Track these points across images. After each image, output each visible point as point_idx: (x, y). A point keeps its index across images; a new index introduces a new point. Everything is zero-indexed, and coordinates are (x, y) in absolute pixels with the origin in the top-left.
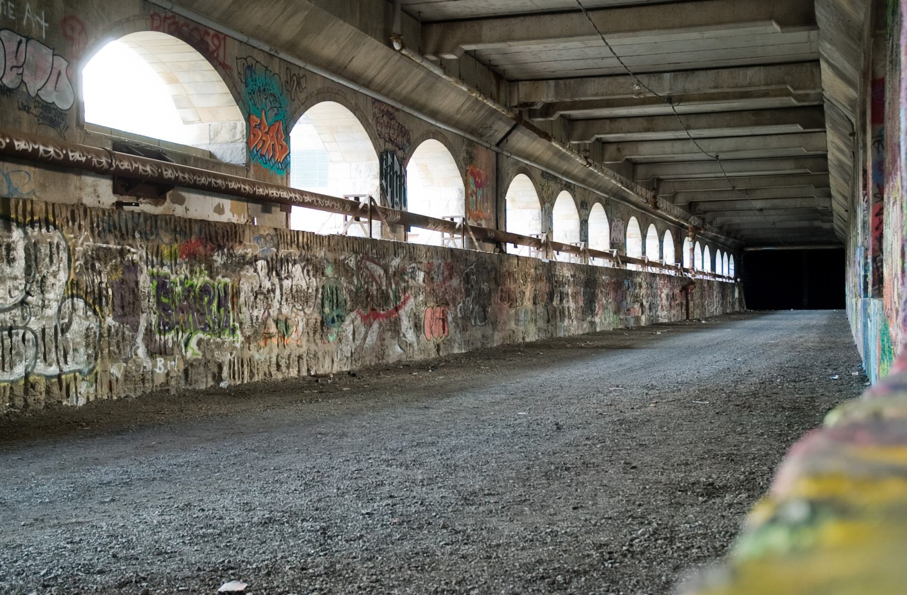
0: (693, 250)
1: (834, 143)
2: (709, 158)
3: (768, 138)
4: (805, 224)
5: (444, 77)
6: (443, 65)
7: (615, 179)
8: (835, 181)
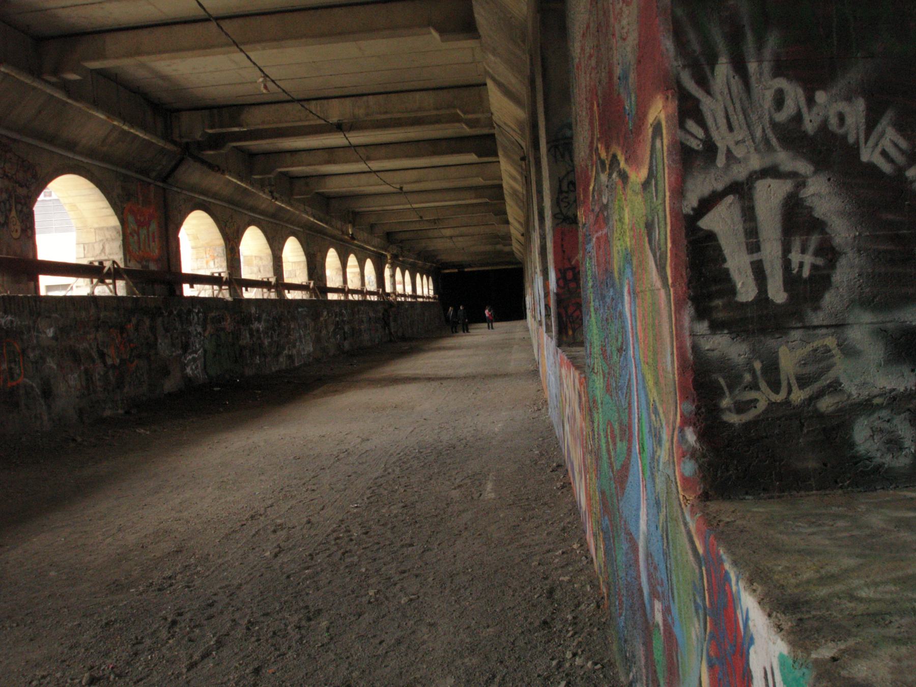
0: (393, 276)
1: (508, 171)
2: (395, 190)
3: (448, 168)
4: (488, 248)
5: (69, 101)
6: (66, 87)
7: (307, 213)
8: (513, 211)
